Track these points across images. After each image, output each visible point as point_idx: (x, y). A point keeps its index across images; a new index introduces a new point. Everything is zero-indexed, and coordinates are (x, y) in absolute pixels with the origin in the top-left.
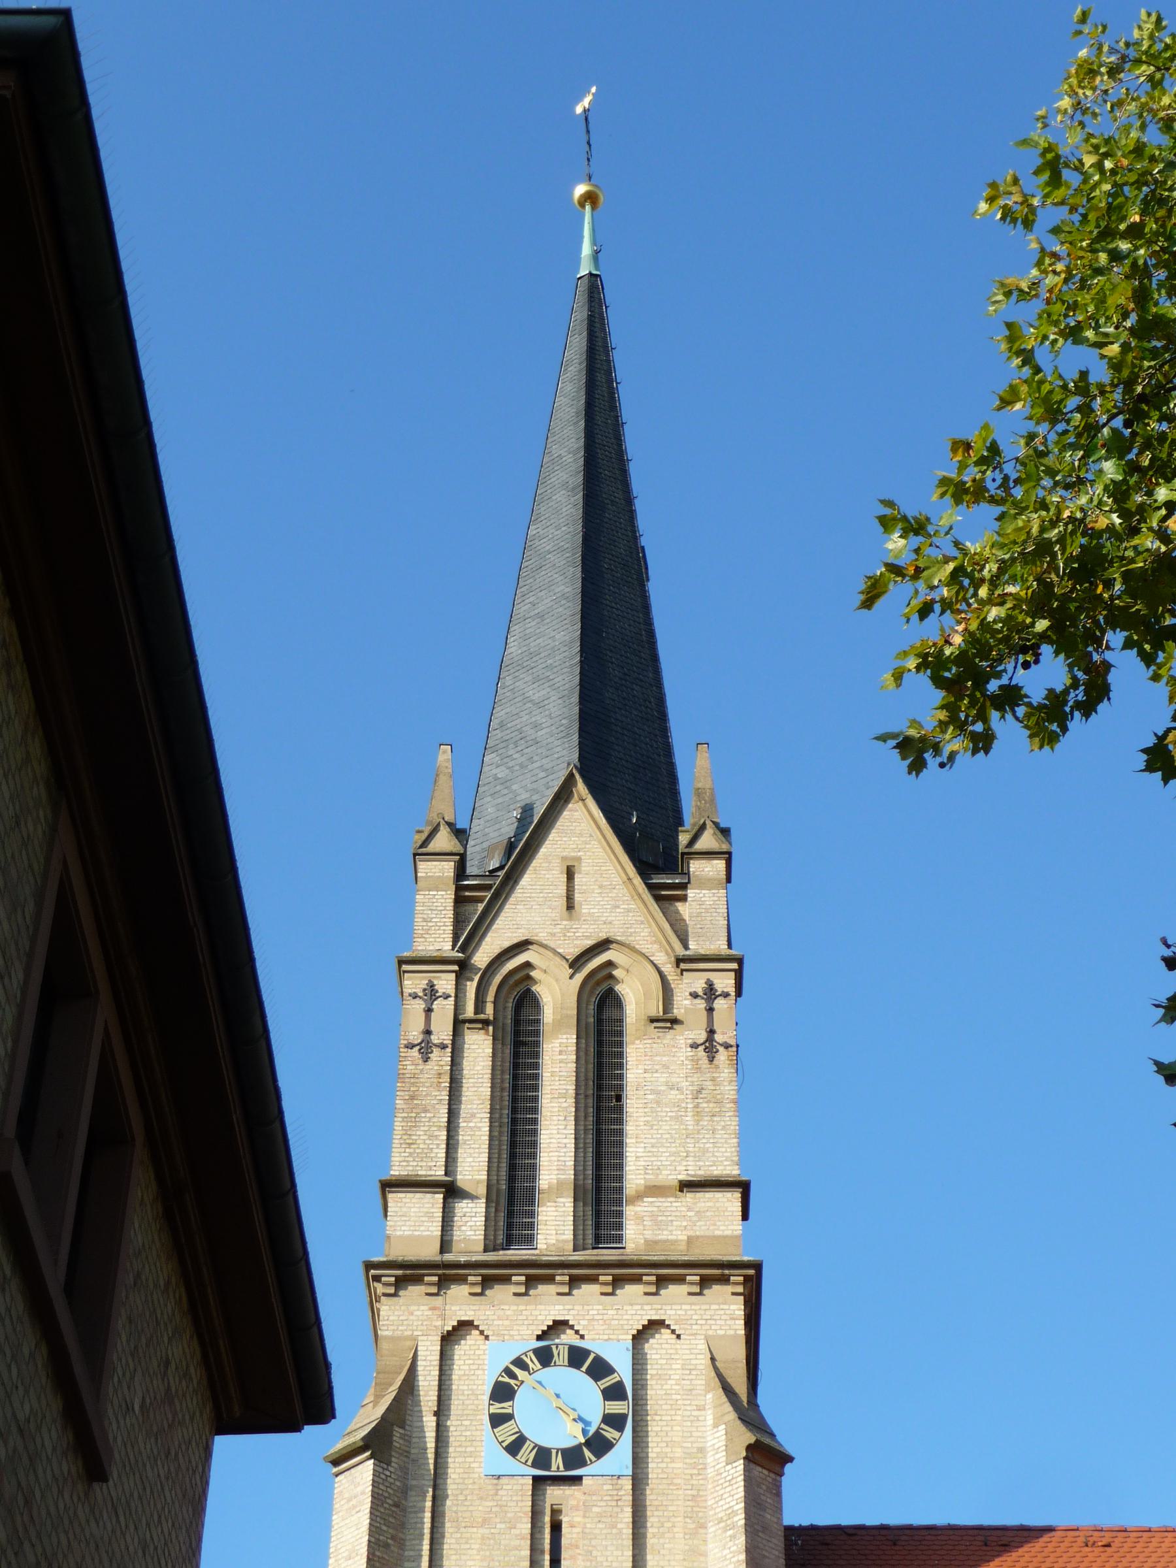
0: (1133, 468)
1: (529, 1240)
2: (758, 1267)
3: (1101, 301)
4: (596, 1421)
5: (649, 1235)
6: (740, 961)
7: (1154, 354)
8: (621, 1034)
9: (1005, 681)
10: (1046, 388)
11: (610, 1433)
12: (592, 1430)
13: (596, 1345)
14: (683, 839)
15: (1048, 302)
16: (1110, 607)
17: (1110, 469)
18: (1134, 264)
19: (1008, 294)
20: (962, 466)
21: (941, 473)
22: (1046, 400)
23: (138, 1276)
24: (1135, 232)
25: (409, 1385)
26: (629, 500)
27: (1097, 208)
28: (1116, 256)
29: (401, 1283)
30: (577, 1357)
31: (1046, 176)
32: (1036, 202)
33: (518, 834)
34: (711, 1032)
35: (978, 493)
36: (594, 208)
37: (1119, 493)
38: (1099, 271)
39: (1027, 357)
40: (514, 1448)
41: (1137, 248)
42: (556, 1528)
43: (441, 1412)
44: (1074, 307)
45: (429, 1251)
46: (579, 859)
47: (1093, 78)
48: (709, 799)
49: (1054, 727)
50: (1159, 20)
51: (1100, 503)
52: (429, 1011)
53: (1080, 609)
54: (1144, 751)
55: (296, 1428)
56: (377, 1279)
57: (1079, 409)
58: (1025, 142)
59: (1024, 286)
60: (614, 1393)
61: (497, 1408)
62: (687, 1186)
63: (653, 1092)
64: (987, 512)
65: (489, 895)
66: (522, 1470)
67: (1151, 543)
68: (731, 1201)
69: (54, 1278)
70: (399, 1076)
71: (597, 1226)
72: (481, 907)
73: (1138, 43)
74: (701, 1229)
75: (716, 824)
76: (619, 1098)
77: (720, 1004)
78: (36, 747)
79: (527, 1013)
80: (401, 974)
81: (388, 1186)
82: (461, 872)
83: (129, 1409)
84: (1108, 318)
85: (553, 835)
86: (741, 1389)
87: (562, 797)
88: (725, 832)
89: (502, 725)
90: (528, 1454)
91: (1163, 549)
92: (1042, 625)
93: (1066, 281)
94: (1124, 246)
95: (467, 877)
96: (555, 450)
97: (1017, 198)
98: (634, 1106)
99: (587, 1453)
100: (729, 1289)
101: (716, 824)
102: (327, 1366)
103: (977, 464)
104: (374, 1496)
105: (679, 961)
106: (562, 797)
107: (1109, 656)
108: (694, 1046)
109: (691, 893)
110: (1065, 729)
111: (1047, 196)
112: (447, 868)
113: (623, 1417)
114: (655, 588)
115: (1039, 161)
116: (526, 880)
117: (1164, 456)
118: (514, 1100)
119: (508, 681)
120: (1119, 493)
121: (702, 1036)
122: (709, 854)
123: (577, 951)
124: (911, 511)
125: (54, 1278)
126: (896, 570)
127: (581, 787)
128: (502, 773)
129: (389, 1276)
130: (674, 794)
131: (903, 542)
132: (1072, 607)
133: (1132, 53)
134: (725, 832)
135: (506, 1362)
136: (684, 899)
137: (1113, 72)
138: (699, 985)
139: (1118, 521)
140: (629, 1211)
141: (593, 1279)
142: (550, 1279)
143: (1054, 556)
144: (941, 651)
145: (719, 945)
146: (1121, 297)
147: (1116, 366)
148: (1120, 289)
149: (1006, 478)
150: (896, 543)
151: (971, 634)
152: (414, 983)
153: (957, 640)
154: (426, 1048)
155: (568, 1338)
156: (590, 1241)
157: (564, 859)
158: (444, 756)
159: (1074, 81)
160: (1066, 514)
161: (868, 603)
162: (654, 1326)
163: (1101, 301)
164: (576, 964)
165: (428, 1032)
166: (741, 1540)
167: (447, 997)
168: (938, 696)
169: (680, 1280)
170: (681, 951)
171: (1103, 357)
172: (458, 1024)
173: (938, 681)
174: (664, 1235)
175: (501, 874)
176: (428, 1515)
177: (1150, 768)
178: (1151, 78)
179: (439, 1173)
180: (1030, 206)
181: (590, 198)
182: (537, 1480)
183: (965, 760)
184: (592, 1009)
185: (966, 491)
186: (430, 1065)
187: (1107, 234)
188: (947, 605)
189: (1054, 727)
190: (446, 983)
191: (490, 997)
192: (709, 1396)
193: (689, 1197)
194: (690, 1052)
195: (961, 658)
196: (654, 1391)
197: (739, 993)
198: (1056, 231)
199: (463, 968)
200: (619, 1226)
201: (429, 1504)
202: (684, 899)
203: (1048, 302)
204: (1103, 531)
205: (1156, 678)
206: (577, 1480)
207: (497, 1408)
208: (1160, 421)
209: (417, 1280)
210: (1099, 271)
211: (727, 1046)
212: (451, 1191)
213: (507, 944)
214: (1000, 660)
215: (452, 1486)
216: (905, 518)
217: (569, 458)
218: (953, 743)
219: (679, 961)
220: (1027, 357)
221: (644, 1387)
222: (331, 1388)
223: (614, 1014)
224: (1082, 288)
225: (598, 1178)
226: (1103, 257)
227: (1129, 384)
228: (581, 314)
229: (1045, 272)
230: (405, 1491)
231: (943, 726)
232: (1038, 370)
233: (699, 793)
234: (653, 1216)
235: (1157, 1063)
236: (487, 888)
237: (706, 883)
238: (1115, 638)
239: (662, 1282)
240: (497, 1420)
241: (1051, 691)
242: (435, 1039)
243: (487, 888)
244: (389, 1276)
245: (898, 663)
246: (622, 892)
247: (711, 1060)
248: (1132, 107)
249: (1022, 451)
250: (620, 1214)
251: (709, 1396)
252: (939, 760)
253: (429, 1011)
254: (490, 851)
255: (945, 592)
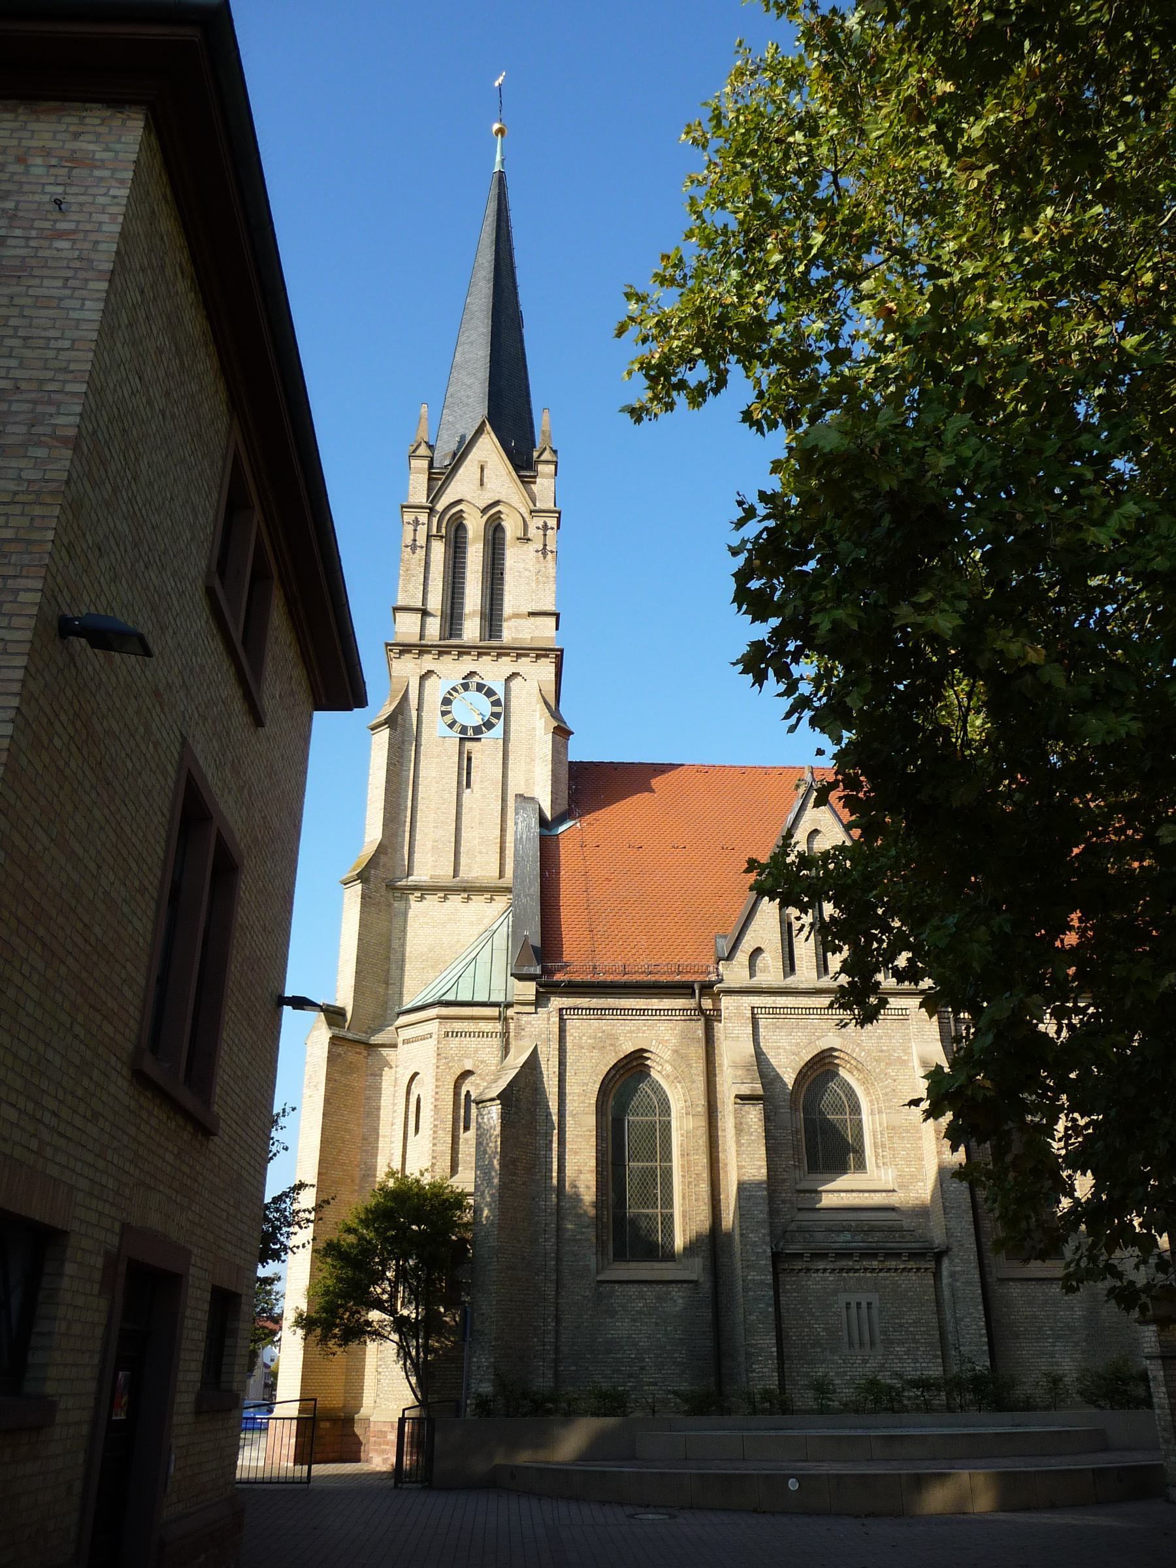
0: (746, 274)
1: (460, 636)
2: (562, 651)
3: (735, 190)
4: (488, 715)
5: (514, 635)
6: (560, 513)
7: (760, 218)
8: (503, 544)
9: (680, 376)
10: (707, 231)
11: (494, 721)
12: (486, 719)
13: (488, 682)
14: (535, 454)
15: (711, 187)
16: (731, 342)
17: (735, 274)
18: (752, 171)
19: (692, 182)
20: (665, 268)
21: (655, 270)
22: (707, 238)
23: (277, 638)
24: (753, 154)
25: (405, 697)
26: (515, 288)
27: (737, 141)
28: (744, 166)
29: (401, 653)
30: (480, 687)
31: (714, 122)
32: (709, 136)
33: (458, 449)
34: (545, 545)
35: (672, 281)
36: (502, 137)
37: (739, 286)
38: (736, 174)
39: (699, 215)
40: (451, 726)
41: (754, 163)
42: (469, 759)
43: (419, 709)
44: (722, 191)
45: (415, 639)
46: (486, 462)
47: (742, 77)
48: (548, 436)
49: (701, 399)
50: (777, 48)
51: (728, 292)
52: (415, 530)
53: (716, 343)
54: (742, 412)
55: (351, 710)
56: (391, 650)
57: (722, 243)
58: (705, 104)
59: (700, 178)
60: (496, 703)
61: (444, 708)
62: (532, 614)
63: (518, 571)
64: (676, 291)
65: (444, 477)
66: (455, 735)
67: (749, 309)
68: (551, 621)
69: (237, 636)
70: (401, 560)
71: (491, 631)
72: (440, 483)
73: (766, 60)
74: (537, 634)
75: (551, 448)
76: (502, 574)
77: (549, 532)
78: (221, 386)
79: (460, 533)
80: (403, 512)
81: (396, 609)
82: (431, 466)
83: (274, 697)
84: (739, 198)
85: (474, 450)
86: (553, 704)
87: (480, 431)
88: (555, 452)
89: (451, 395)
90: (457, 728)
91: (755, 313)
92: (698, 351)
93: (720, 177)
94: (749, 161)
95: (434, 468)
96: (480, 260)
97: (700, 133)
98: (508, 577)
99: (484, 728)
100: (549, 660)
101: (551, 448)
102: (364, 683)
103: (672, 267)
104: (389, 744)
105: (531, 512)
106: (480, 431)
107: (728, 366)
108: (537, 551)
109: (538, 480)
110: (705, 401)
111: (714, 133)
112: (425, 464)
113: (500, 714)
114: (525, 332)
115: (711, 115)
116: (461, 471)
117: (760, 269)
118: (454, 573)
119: (455, 374)
120: (739, 286)
121: (541, 547)
122: (547, 462)
123: (485, 505)
124: (640, 291)
125: (237, 636)
126: (632, 319)
127: (488, 426)
128: (451, 419)
129: (397, 649)
130: (532, 433)
131: (636, 306)
132: (712, 342)
133: (763, 65)
134: (555, 452)
135: (449, 689)
136: (535, 483)
137: (753, 74)
138: (540, 524)
139: (736, 300)
140: (505, 624)
141: (488, 654)
142: (469, 653)
143: (705, 316)
144: (650, 361)
145: (551, 506)
146: (745, 187)
147: (741, 223)
148: (744, 183)
149: (685, 275)
150: (633, 307)
151: (665, 353)
152: (409, 517)
153: (657, 356)
154: (414, 548)
155: (476, 679)
156: (487, 637)
157: (479, 461)
158: (424, 409)
159: (733, 77)
160: (712, 295)
161: (619, 335)
162: (515, 675)
163: (735, 190)
164: (484, 511)
165: (415, 540)
166: (550, 766)
167: (423, 524)
168: (647, 383)
169: (527, 655)
170: (533, 508)
171: (736, 218)
172: (429, 537)
173: (647, 376)
174: (521, 636)
175: (450, 467)
176: (413, 752)
177: (744, 421)
178: (771, 79)
179: (419, 605)
180: (706, 138)
181: (501, 131)
182: (461, 739)
183: (662, 415)
184: (491, 532)
185: (667, 280)
186: (415, 555)
187: (739, 154)
188: (655, 338)
189: (701, 399)
190: (423, 518)
191: (444, 525)
192: (538, 706)
193: (532, 619)
194: (535, 554)
195: (658, 366)
196: (514, 703)
197: (558, 528)
198: (717, 151)
199: (432, 511)
200: (501, 631)
201: (414, 748)
202: (535, 483)
203: (711, 187)
204: (728, 305)
205: (748, 377)
206: (479, 739)
207: (444, 708)
208: (760, 252)
209: (409, 652)
210: (736, 174)
211: (552, 552)
212: (425, 613)
213: (452, 501)
214: (678, 366)
215: (423, 741)
216: (637, 294)
217: (487, 264)
218: (656, 408)
219: (531, 512)
220: (699, 215)
221: (510, 701)
222: (366, 693)
223: (501, 535)
224: (728, 181)
225: (491, 610)
226: (738, 166)
227: (747, 232)
228: (494, 192)
229: (710, 172)
230: (403, 742)
231: (652, 400)
232: (704, 222)
233: (543, 432)
234: (516, 627)
235: (729, 546)
236: (443, 474)
237: (545, 476)
238: (733, 358)
239: (519, 656)
240: (444, 713)
241: (700, 382)
242: (418, 543)
243: (443, 474)
244: (397, 649)
245: (630, 367)
246: (506, 479)
247: (545, 558)
248: (761, 94)
249: (695, 263)
250: (501, 626)
251: (538, 706)
252: (648, 417)
253: (415, 530)
254: (445, 456)
255: (654, 331)
